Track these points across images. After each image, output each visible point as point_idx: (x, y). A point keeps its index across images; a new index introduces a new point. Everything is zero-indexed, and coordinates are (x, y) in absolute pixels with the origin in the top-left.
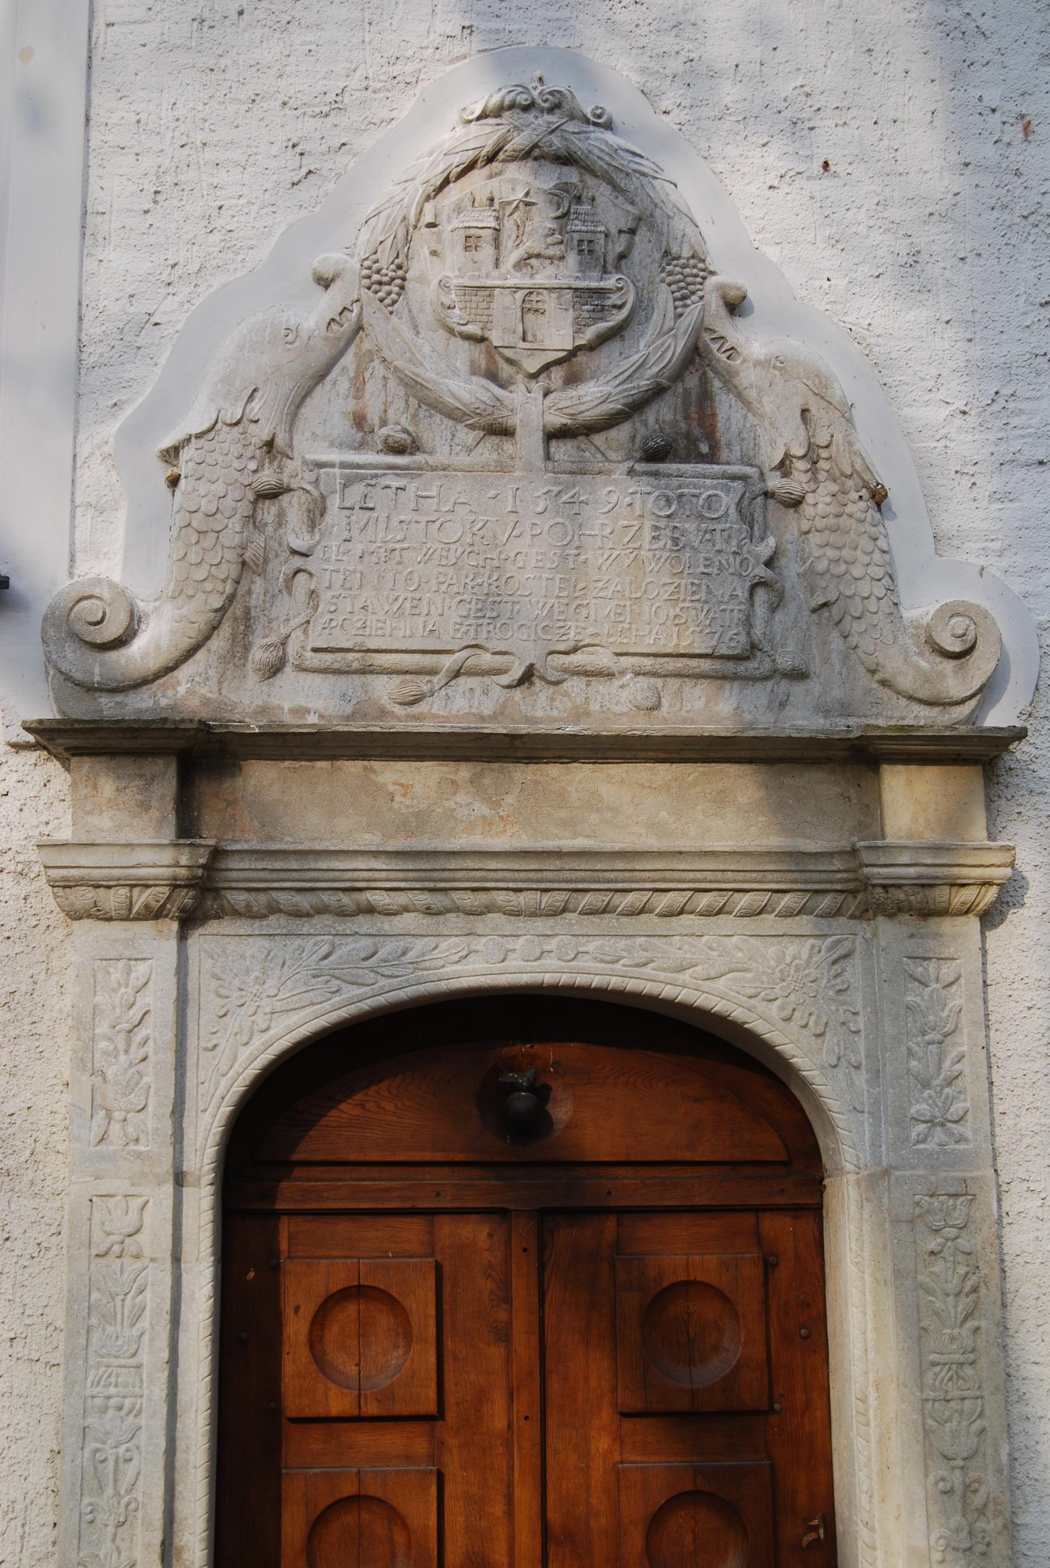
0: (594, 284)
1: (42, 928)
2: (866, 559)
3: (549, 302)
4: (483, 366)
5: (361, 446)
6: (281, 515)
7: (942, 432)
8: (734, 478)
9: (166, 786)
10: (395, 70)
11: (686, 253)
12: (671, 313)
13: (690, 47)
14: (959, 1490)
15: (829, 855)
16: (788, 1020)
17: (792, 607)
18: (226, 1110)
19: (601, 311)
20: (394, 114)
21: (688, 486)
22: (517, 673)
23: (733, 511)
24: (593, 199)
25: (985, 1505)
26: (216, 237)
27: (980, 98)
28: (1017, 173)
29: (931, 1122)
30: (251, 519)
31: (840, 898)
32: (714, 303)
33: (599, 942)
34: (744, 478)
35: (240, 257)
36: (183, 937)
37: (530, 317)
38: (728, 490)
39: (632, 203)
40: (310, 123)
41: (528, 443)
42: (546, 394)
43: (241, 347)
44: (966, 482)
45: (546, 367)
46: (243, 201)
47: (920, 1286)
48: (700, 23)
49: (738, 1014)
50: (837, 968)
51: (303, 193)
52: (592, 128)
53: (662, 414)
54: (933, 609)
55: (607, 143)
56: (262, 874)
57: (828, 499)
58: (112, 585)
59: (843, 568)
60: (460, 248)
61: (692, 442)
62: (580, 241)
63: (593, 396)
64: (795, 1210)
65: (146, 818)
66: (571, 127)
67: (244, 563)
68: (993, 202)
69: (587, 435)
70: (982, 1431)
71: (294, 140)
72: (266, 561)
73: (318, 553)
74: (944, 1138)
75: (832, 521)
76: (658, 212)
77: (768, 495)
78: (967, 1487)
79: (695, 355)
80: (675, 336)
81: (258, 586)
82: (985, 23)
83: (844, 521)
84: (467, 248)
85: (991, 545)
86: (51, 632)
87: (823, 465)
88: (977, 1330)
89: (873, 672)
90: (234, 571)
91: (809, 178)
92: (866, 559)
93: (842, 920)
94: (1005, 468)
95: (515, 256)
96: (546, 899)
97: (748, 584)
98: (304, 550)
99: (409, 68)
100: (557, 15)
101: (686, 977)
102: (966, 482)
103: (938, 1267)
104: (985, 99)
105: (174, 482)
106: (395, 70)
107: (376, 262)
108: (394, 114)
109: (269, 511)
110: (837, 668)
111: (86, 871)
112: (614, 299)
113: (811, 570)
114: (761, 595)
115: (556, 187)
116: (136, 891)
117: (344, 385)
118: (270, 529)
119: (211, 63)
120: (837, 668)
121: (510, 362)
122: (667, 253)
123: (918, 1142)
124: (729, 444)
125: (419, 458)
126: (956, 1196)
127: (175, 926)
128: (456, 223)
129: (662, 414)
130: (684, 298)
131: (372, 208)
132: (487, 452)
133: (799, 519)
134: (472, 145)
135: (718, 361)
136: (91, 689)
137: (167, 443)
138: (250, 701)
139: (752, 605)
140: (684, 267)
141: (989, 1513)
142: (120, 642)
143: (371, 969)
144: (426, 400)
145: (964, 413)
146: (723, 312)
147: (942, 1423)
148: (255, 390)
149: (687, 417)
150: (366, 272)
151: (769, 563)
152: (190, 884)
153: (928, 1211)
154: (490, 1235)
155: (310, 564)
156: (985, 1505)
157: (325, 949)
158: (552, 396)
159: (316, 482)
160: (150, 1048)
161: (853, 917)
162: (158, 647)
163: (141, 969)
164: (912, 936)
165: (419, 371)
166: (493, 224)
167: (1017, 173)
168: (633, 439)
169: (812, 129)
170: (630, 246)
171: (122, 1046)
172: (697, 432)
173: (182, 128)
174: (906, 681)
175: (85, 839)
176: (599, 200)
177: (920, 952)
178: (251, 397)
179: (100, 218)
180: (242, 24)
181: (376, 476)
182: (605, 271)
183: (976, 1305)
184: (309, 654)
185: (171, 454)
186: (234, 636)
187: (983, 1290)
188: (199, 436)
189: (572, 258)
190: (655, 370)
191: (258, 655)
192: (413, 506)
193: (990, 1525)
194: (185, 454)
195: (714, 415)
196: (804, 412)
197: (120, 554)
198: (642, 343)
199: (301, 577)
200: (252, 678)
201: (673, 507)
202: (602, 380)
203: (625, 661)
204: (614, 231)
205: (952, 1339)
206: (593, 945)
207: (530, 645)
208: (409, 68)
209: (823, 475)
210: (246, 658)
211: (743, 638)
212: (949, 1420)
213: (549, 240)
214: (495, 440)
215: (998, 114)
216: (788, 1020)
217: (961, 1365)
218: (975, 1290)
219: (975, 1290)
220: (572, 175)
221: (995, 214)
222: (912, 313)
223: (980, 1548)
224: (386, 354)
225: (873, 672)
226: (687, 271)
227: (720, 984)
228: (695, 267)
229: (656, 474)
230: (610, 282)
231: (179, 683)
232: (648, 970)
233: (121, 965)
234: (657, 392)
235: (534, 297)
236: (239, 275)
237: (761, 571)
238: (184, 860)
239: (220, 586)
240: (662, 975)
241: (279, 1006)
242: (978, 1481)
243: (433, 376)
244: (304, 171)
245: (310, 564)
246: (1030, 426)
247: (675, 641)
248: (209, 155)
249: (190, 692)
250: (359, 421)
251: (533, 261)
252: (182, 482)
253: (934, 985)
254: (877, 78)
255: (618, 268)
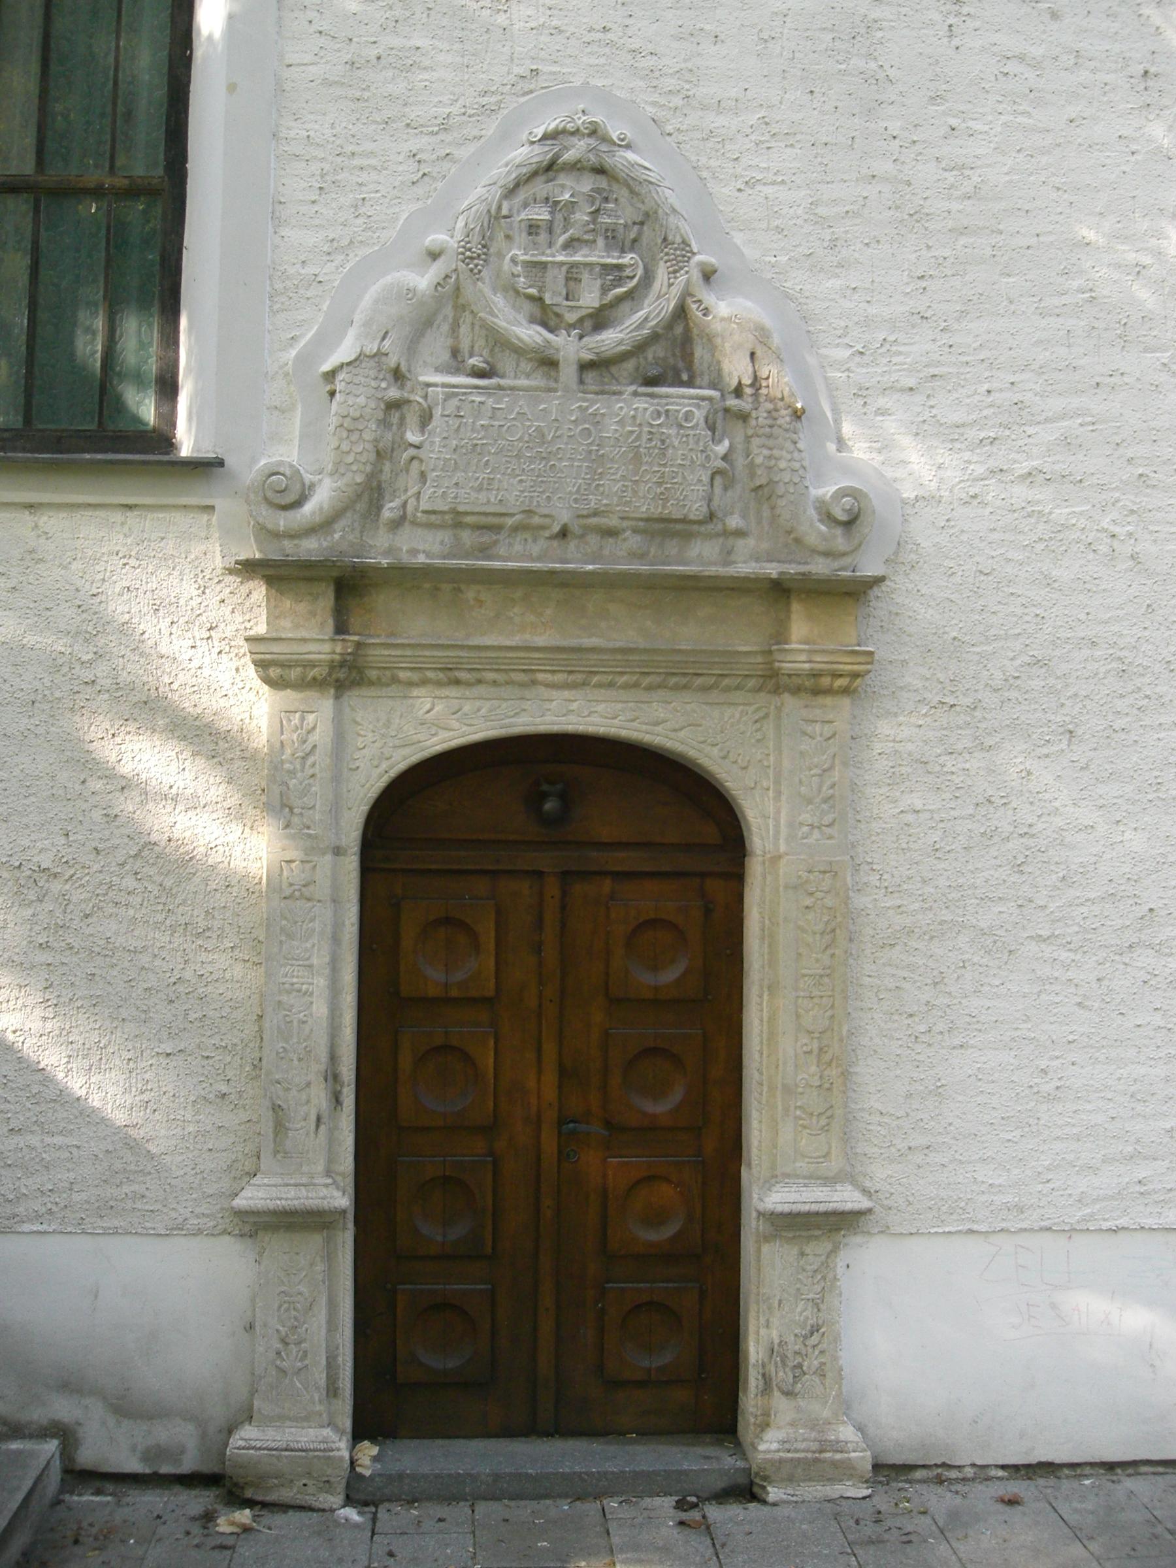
0: (615, 261)
1: (247, 688)
2: (789, 456)
3: (585, 276)
4: (539, 316)
5: (457, 371)
6: (402, 419)
7: (847, 366)
8: (703, 399)
9: (327, 601)
10: (484, 100)
11: (678, 240)
12: (666, 283)
13: (687, 87)
14: (816, 1051)
15: (756, 653)
16: (724, 758)
17: (738, 488)
18: (365, 808)
19: (619, 281)
20: (483, 132)
21: (672, 404)
22: (556, 528)
23: (702, 421)
24: (616, 200)
25: (831, 1060)
26: (360, 221)
27: (886, 129)
28: (909, 184)
29: (812, 826)
30: (384, 423)
31: (761, 680)
32: (696, 275)
33: (603, 706)
34: (710, 399)
35: (375, 236)
36: (337, 697)
37: (572, 283)
38: (698, 407)
39: (643, 203)
40: (425, 139)
41: (568, 373)
42: (581, 337)
43: (376, 301)
44: (860, 401)
45: (581, 320)
46: (378, 195)
47: (799, 927)
48: (695, 69)
49: (692, 753)
50: (758, 725)
51: (419, 190)
52: (616, 149)
53: (657, 351)
54: (834, 489)
55: (627, 160)
56: (388, 659)
57: (765, 415)
58: (291, 466)
59: (773, 462)
60: (524, 234)
61: (677, 373)
62: (607, 230)
63: (611, 339)
64: (727, 876)
65: (313, 621)
66: (604, 147)
67: (378, 453)
68: (890, 203)
69: (607, 367)
70: (832, 1016)
71: (414, 151)
72: (392, 450)
73: (427, 446)
74: (819, 837)
75: (768, 430)
76: (660, 211)
77: (727, 410)
78: (821, 1049)
79: (681, 312)
80: (668, 299)
81: (387, 467)
82: (892, 73)
83: (776, 430)
84: (530, 234)
85: (874, 445)
86: (252, 496)
87: (764, 391)
88: (833, 955)
89: (789, 532)
90: (372, 457)
91: (765, 184)
92: (789, 456)
93: (762, 694)
94: (887, 392)
95: (562, 240)
96: (571, 678)
97: (709, 472)
98: (417, 444)
99: (493, 99)
100: (597, 61)
101: (659, 729)
102: (860, 401)
103: (811, 916)
104: (890, 128)
105: (332, 394)
106: (484, 100)
107: (469, 242)
108: (483, 132)
109: (395, 418)
110: (766, 529)
111: (275, 656)
112: (628, 272)
113: (752, 463)
114: (718, 480)
115: (592, 190)
116: (308, 669)
117: (445, 328)
118: (394, 427)
119: (358, 94)
120: (766, 529)
121: (558, 315)
122: (665, 239)
123: (804, 838)
124: (702, 374)
125: (494, 381)
126: (825, 872)
127: (332, 691)
128: (523, 216)
129: (657, 351)
130: (675, 272)
131: (466, 203)
132: (538, 381)
133: (745, 428)
134: (535, 160)
135: (697, 316)
136: (277, 535)
137: (326, 367)
138: (381, 548)
139: (712, 486)
140: (676, 249)
141: (834, 1064)
142: (298, 504)
143: (458, 720)
144: (499, 342)
145: (861, 353)
146: (701, 281)
147: (807, 1011)
148: (387, 333)
149: (674, 355)
150: (461, 250)
151: (725, 458)
152: (342, 664)
153: (806, 882)
154: (531, 887)
155: (422, 453)
156: (831, 1060)
157: (428, 706)
158: (585, 339)
159: (426, 397)
160: (317, 770)
161: (769, 692)
162: (321, 509)
163: (311, 718)
164: (806, 706)
165: (496, 320)
166: (548, 217)
167: (909, 184)
168: (637, 369)
169: (769, 148)
170: (640, 234)
171: (298, 767)
172: (681, 365)
173: (338, 142)
174: (812, 540)
175: (274, 635)
176: (622, 200)
177: (811, 717)
178: (383, 339)
179: (282, 206)
180: (380, 67)
181: (464, 394)
182: (623, 251)
183: (833, 940)
184: (419, 514)
185: (331, 376)
186: (371, 501)
187: (838, 931)
188: (349, 364)
189: (601, 242)
190: (654, 322)
191: (387, 514)
192: (489, 414)
193: (834, 1072)
194: (341, 376)
195: (692, 354)
196: (752, 354)
197: (296, 442)
198: (647, 302)
199: (415, 463)
200: (382, 531)
201: (662, 419)
202: (618, 329)
203: (625, 524)
204: (630, 222)
205: (817, 960)
206: (601, 708)
207: (565, 511)
208: (493, 99)
209: (762, 399)
210: (378, 516)
211: (705, 509)
212: (812, 1009)
213: (586, 229)
214: (546, 369)
215: (897, 141)
216: (724, 758)
217: (821, 976)
218: (833, 931)
219: (833, 931)
220: (603, 182)
221: (891, 212)
222: (831, 282)
223: (827, 1085)
224: (473, 307)
225: (789, 532)
226: (678, 252)
227: (682, 734)
228: (683, 249)
229: (652, 396)
230: (627, 259)
231: (335, 532)
232: (635, 724)
233: (298, 715)
234: (654, 337)
235: (574, 270)
236: (376, 248)
237: (720, 464)
238: (338, 649)
239: (362, 467)
240: (644, 727)
241: (397, 743)
242: (828, 1046)
243: (504, 324)
244: (421, 173)
245: (422, 453)
246: (905, 364)
247: (660, 510)
248: (357, 162)
249: (342, 537)
250: (455, 352)
251: (576, 244)
252: (338, 395)
253: (819, 738)
254: (816, 112)
255: (632, 249)
